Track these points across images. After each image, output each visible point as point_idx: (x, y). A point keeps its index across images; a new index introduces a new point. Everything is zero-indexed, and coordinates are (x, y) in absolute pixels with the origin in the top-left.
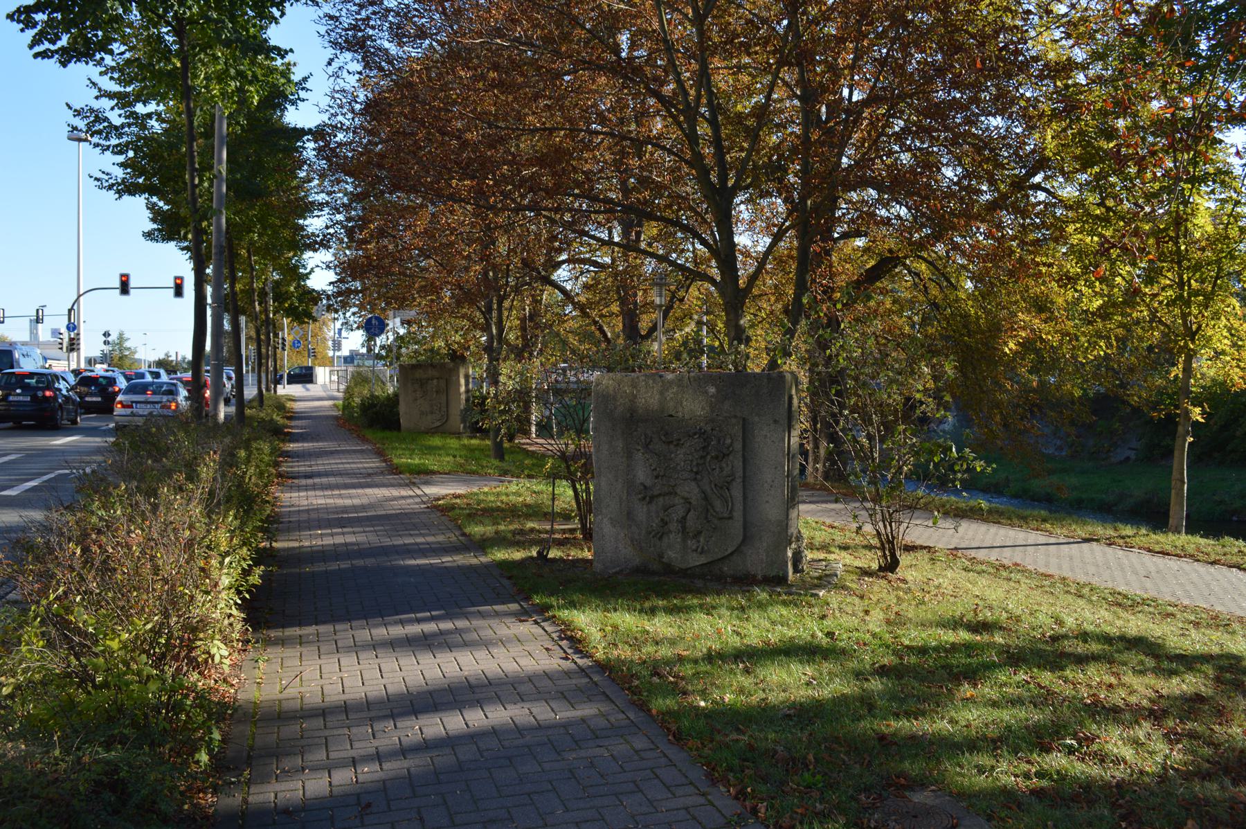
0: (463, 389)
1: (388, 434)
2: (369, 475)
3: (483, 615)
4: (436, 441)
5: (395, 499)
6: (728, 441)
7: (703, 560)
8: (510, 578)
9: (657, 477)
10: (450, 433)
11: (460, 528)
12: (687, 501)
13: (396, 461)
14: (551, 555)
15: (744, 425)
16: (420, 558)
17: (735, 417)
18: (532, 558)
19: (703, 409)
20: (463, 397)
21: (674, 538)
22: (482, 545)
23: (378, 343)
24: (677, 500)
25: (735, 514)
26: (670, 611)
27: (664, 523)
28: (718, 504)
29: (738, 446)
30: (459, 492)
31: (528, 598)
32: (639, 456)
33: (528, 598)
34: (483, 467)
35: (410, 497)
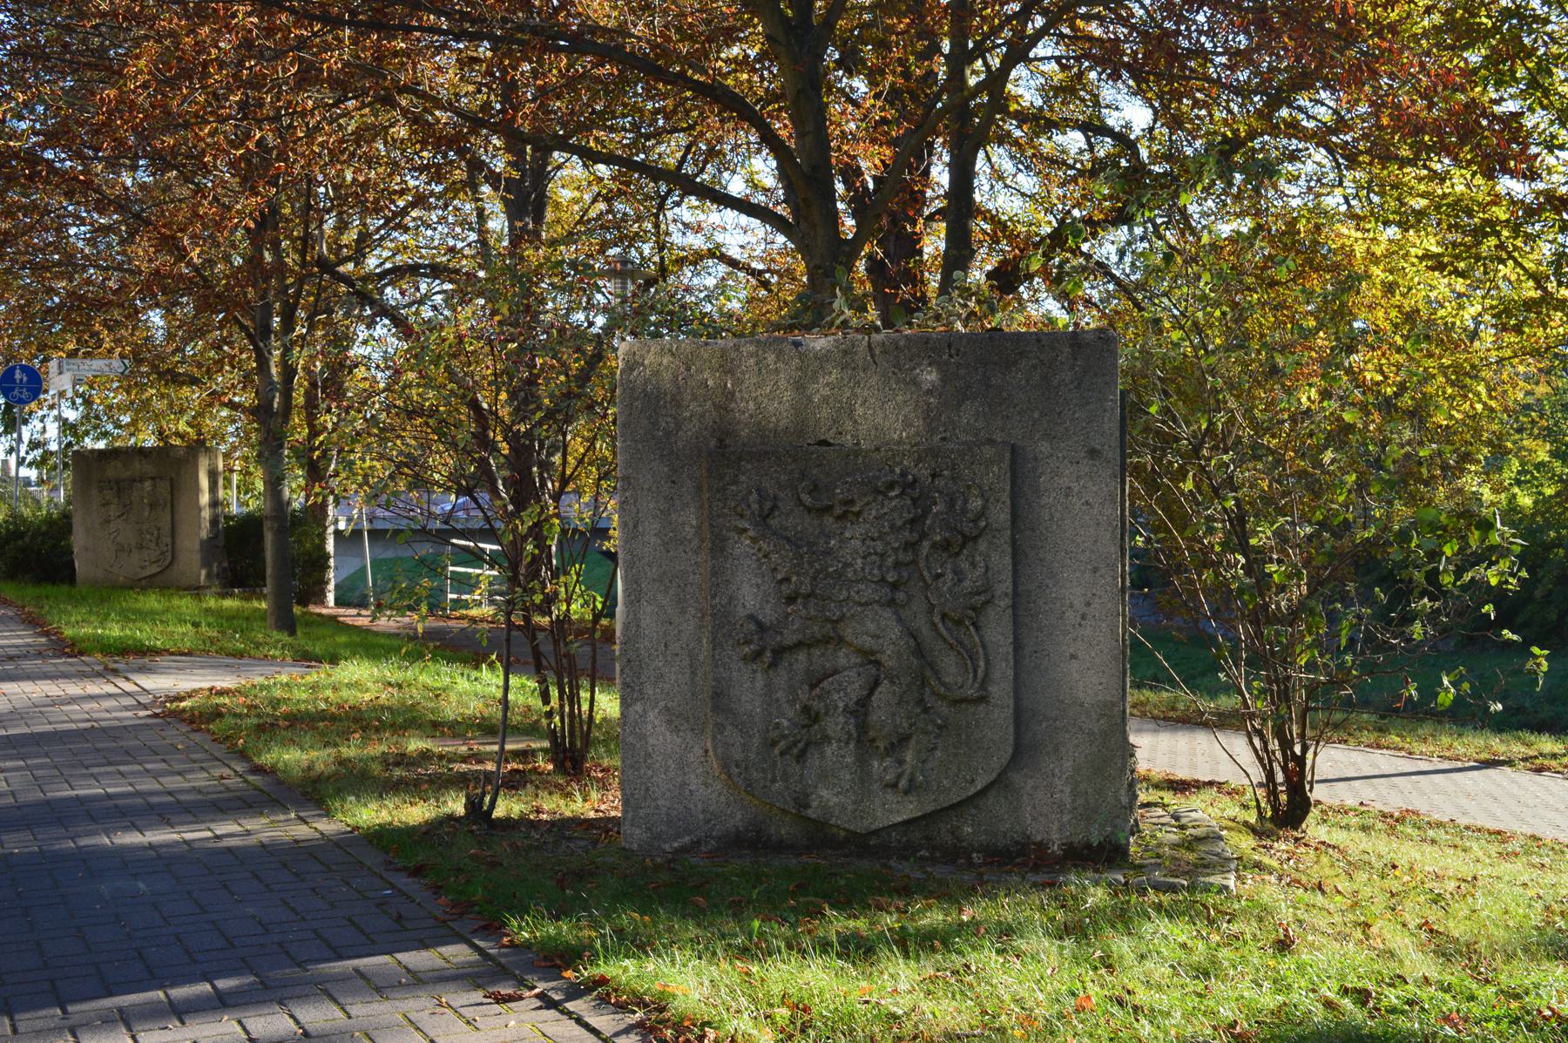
0: (205, 499)
1: (49, 589)
2: (11, 658)
3: (379, 987)
4: (152, 602)
5: (73, 700)
6: (976, 504)
7: (908, 809)
8: (417, 872)
9: (791, 600)
10: (178, 588)
11: (243, 755)
12: (869, 657)
13: (69, 632)
14: (499, 812)
15: (1013, 462)
16: (151, 826)
17: (991, 442)
18: (451, 818)
19: (907, 424)
20: (206, 514)
21: (837, 755)
22: (313, 793)
23: (26, 437)
24: (843, 658)
25: (993, 689)
26: (910, 943)
27: (811, 717)
28: (949, 665)
29: (1000, 515)
30: (219, 685)
31: (493, 928)
32: (742, 546)
33: (493, 928)
34: (258, 645)
35: (110, 696)
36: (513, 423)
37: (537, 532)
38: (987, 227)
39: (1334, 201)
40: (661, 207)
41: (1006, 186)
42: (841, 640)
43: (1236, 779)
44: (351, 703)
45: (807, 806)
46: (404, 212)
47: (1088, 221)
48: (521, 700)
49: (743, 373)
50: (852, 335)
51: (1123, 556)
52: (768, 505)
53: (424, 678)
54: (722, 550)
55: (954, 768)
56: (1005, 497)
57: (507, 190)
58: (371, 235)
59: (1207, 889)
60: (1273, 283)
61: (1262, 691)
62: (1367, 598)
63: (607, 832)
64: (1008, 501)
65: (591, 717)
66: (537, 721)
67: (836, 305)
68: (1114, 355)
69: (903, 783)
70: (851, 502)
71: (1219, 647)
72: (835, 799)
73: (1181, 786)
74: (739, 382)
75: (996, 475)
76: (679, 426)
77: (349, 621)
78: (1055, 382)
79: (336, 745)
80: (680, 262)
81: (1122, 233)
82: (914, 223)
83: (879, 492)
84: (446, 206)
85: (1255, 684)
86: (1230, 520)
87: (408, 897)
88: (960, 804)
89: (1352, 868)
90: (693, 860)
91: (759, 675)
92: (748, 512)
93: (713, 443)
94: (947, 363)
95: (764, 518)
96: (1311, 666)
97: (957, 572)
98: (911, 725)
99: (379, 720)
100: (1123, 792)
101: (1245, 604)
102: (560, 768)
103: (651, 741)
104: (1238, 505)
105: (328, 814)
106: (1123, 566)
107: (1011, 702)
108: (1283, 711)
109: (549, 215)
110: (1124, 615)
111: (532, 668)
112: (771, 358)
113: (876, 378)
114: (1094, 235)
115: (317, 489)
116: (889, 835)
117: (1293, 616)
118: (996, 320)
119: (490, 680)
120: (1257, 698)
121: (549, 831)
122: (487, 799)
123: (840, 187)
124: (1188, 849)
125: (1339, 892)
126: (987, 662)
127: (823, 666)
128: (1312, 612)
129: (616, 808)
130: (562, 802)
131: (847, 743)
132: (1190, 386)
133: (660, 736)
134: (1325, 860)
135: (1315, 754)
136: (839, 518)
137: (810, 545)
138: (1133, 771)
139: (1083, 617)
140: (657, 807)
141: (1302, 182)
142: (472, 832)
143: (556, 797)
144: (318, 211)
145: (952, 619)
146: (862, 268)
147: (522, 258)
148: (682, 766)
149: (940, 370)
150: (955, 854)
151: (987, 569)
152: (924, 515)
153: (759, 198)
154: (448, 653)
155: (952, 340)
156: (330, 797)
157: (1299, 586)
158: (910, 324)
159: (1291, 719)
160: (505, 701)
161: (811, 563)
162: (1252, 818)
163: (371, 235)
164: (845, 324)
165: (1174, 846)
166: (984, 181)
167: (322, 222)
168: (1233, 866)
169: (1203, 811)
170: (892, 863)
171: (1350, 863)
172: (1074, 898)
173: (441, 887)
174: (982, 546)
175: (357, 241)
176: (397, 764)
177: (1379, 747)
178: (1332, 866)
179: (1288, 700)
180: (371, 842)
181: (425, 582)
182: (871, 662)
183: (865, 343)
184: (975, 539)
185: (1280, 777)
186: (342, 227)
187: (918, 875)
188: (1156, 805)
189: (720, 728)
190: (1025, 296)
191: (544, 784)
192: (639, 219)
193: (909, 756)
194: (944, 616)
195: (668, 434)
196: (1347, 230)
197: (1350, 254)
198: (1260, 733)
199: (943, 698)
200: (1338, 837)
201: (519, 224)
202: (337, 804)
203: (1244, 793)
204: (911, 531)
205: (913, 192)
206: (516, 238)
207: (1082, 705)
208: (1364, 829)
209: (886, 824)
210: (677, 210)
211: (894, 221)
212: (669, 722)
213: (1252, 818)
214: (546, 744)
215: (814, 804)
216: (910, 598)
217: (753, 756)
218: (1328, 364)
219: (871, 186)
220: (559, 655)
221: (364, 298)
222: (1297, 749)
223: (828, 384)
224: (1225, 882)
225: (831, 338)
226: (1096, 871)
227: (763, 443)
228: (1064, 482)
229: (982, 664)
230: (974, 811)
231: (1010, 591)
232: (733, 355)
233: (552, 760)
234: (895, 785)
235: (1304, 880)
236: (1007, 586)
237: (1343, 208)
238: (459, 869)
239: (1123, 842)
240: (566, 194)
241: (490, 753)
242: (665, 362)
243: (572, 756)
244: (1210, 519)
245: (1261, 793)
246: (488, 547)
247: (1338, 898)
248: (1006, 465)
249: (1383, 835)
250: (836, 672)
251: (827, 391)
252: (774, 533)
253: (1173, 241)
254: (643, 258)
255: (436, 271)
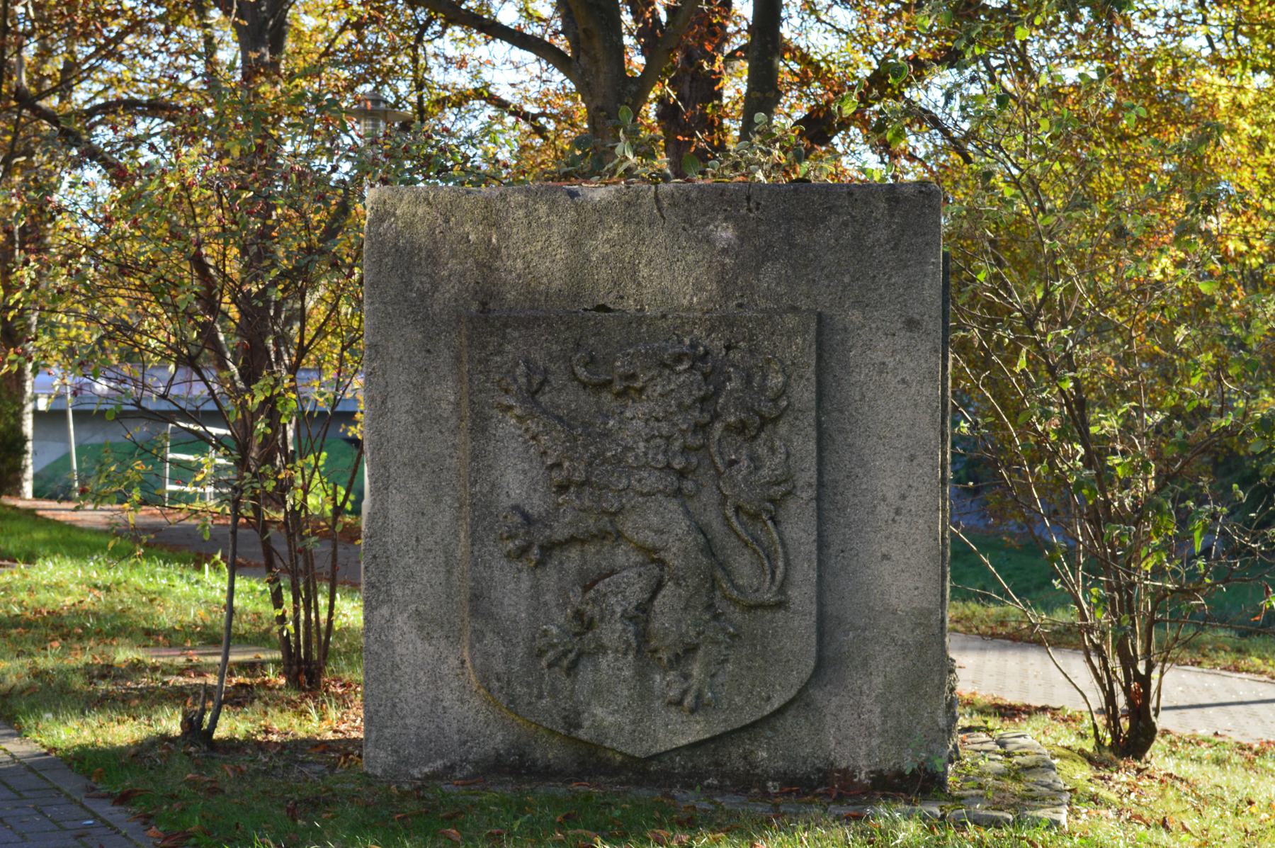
6: (776, 380)
7: (697, 730)
8: (123, 799)
9: (562, 488)
12: (652, 556)
14: (221, 732)
15: (819, 333)
17: (794, 309)
18: (165, 738)
19: (699, 288)
21: (613, 665)
24: (622, 555)
25: (793, 593)
27: (584, 623)
28: (744, 566)
29: (804, 394)
36: (243, 282)
37: (270, 408)
38: (796, 67)
39: (1195, 43)
40: (419, 39)
41: (819, 20)
42: (619, 535)
43: (1073, 705)
44: (50, 607)
45: (579, 726)
46: (120, 36)
47: (915, 61)
48: (250, 607)
49: (510, 226)
50: (637, 184)
51: (944, 441)
52: (537, 379)
53: (137, 579)
54: (484, 430)
55: (747, 683)
56: (810, 373)
57: (240, 14)
58: (79, 65)
59: (1035, 823)
60: (1123, 137)
61: (1102, 600)
62: (1223, 495)
63: (347, 755)
64: (814, 378)
65: (330, 622)
66: (268, 631)
67: (618, 150)
68: (937, 213)
69: (689, 701)
70: (633, 377)
71: (1052, 548)
72: (611, 719)
73: (1009, 712)
74: (505, 237)
75: (801, 348)
76: (435, 288)
77: (49, 514)
78: (869, 243)
79: (31, 655)
80: (441, 103)
81: (949, 76)
82: (712, 60)
83: (665, 366)
84: (167, 32)
85: (1094, 590)
86: (1068, 404)
87: (113, 828)
88: (754, 725)
89: (1202, 802)
90: (447, 788)
91: (524, 575)
92: (514, 387)
93: (474, 307)
94: (744, 218)
95: (533, 394)
96: (1158, 572)
97: (753, 458)
98: (699, 634)
99: (83, 627)
100: (940, 713)
101: (1083, 499)
102: (294, 682)
103: (399, 649)
104: (1078, 387)
105: (20, 733)
106: (944, 454)
107: (814, 608)
108: (1126, 622)
109: (289, 45)
110: (944, 510)
111: (263, 570)
112: (543, 209)
113: (663, 234)
114: (920, 78)
115: (12, 356)
116: (673, 761)
117: (1139, 513)
118: (803, 168)
119: (213, 582)
120: (1096, 606)
121: (280, 754)
122: (208, 717)
123: (627, 18)
124: (1014, 778)
125: (1185, 829)
126: (787, 563)
127: (599, 565)
128: (1159, 509)
129: (358, 728)
130: (295, 721)
131: (625, 654)
132: (1020, 249)
133: (409, 645)
134: (1170, 793)
135: (1162, 673)
136: (619, 395)
137: (585, 425)
138: (952, 690)
139: (898, 512)
140: (405, 727)
141: (1161, 20)
142: (189, 754)
143: (288, 715)
144: (16, 33)
145: (747, 513)
146: (652, 114)
147: (257, 95)
148: (436, 678)
149: (737, 227)
150: (747, 783)
151: (788, 455)
152: (717, 393)
153: (534, 30)
154: (165, 552)
155: (751, 193)
156: (23, 714)
157: (1146, 481)
158: (703, 173)
159: (1134, 632)
160: (230, 609)
161: (585, 447)
162: (1089, 746)
163: (79, 65)
164: (628, 171)
165: (999, 776)
166: (794, 14)
167: (20, 47)
168: (1065, 798)
169: (1031, 737)
170: (675, 792)
171: (1199, 798)
172: (883, 833)
173: (150, 817)
174: (783, 429)
175: (63, 72)
176: (103, 677)
177: (1237, 670)
178: (1179, 800)
179: (1131, 611)
180: (70, 765)
181: (138, 465)
182: (653, 561)
183: (651, 194)
184: (774, 421)
185: (1121, 701)
186: (45, 53)
187: (704, 805)
188: (979, 729)
189: (478, 636)
190: (840, 149)
191: (275, 700)
192: (394, 50)
193: (696, 670)
194: (738, 509)
195: (422, 296)
196: (1211, 77)
197: (1213, 105)
198: (1098, 649)
199: (736, 602)
200: (1188, 770)
201: (253, 55)
202: (32, 722)
203: (1081, 720)
204: (702, 411)
205: (711, 24)
206: (251, 71)
207: (894, 613)
208: (1218, 762)
209: (669, 746)
210: (438, 42)
211: (690, 58)
212: (421, 628)
213: (1089, 746)
214: (278, 655)
215: (587, 724)
216: (699, 488)
217: (516, 668)
218: (1184, 230)
219: (663, 17)
220: (292, 554)
221: (70, 137)
222: (1141, 668)
223: (608, 241)
224: (1055, 817)
225: (612, 188)
226: (908, 802)
227: (532, 308)
228: (878, 356)
229: (781, 564)
230: (769, 734)
231: (814, 481)
232: (500, 205)
233: (285, 673)
234: (679, 703)
235: (1146, 815)
236: (810, 475)
237: (1207, 52)
238: (173, 797)
239: (941, 770)
240: (309, 22)
241: (212, 665)
242: (420, 212)
243: (307, 669)
244: (1044, 402)
245: (1101, 720)
246: (214, 431)
247: (1185, 836)
248: (811, 336)
249: (1241, 770)
250: (612, 572)
251: (606, 249)
252: (544, 412)
253: (1010, 87)
254: (398, 97)
255: (155, 108)
